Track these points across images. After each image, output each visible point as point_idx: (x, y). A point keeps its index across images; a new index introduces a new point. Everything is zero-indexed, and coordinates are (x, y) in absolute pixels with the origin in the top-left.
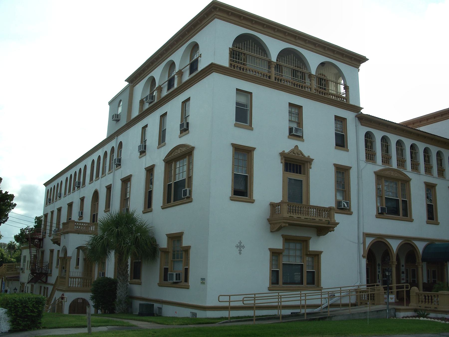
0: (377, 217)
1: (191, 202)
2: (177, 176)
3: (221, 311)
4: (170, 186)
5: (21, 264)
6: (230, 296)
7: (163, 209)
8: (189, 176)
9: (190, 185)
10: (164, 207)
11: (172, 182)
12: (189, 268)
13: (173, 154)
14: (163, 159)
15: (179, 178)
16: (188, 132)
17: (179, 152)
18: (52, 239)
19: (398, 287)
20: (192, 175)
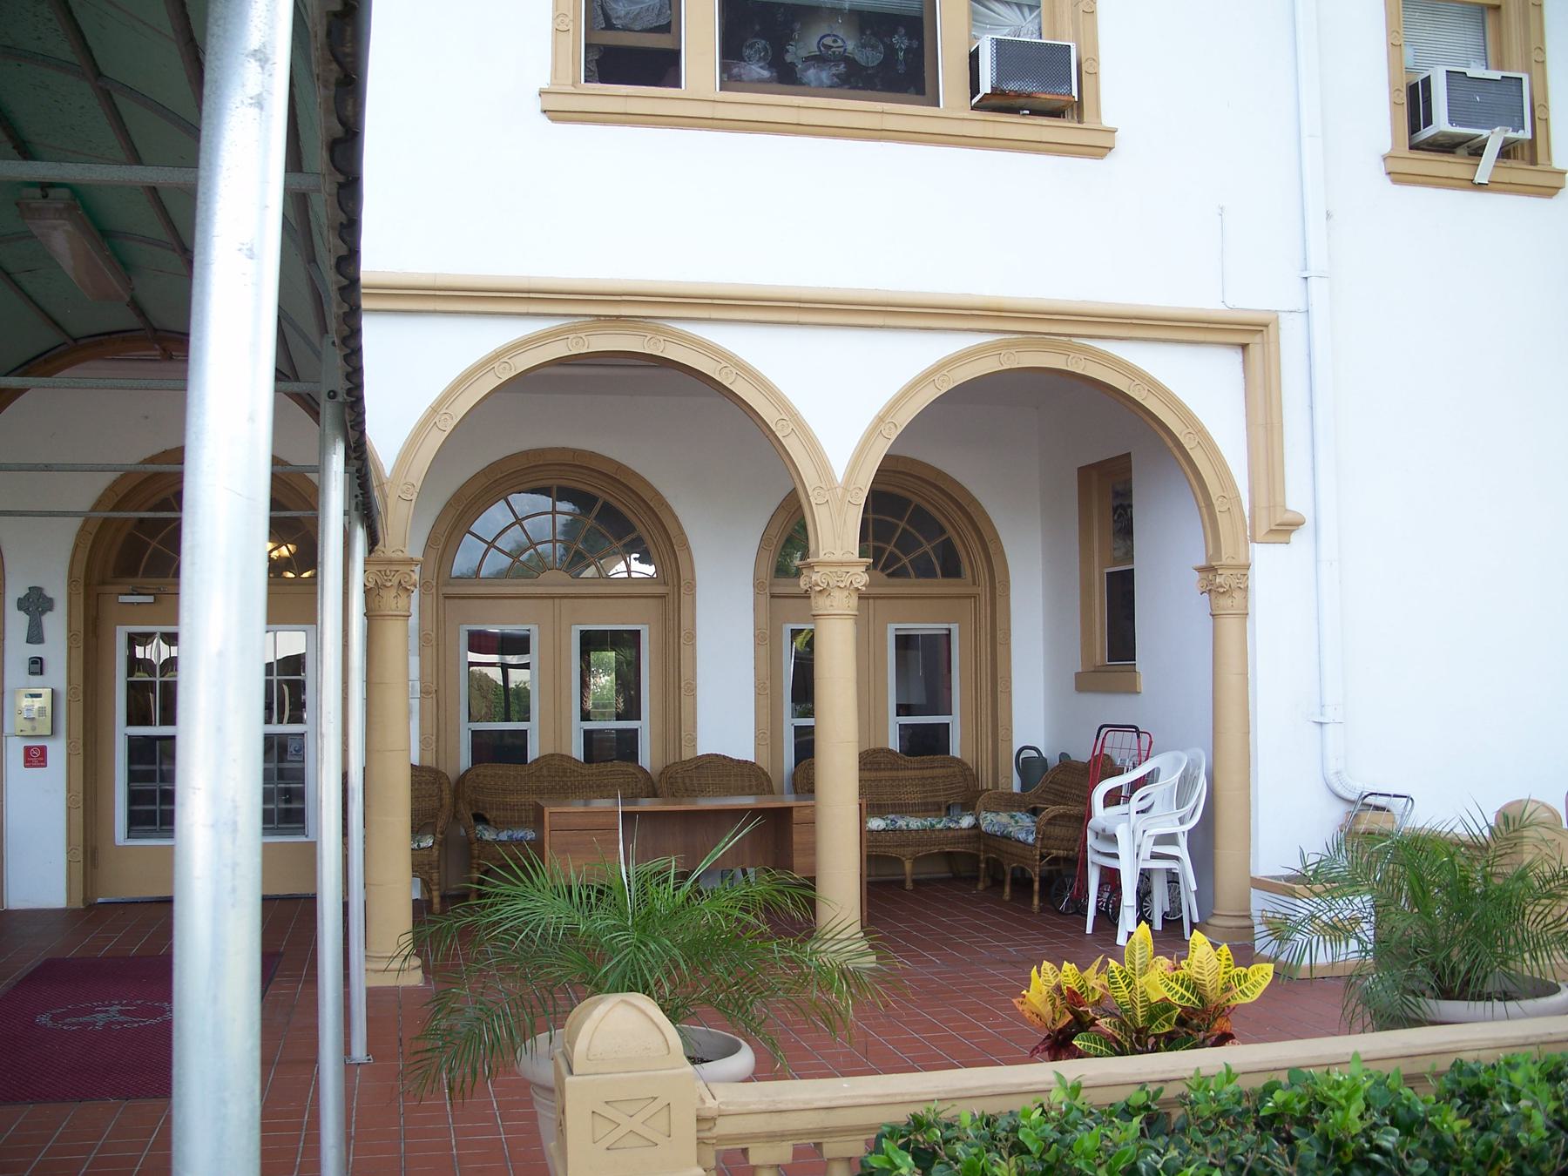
0: (1397, 177)
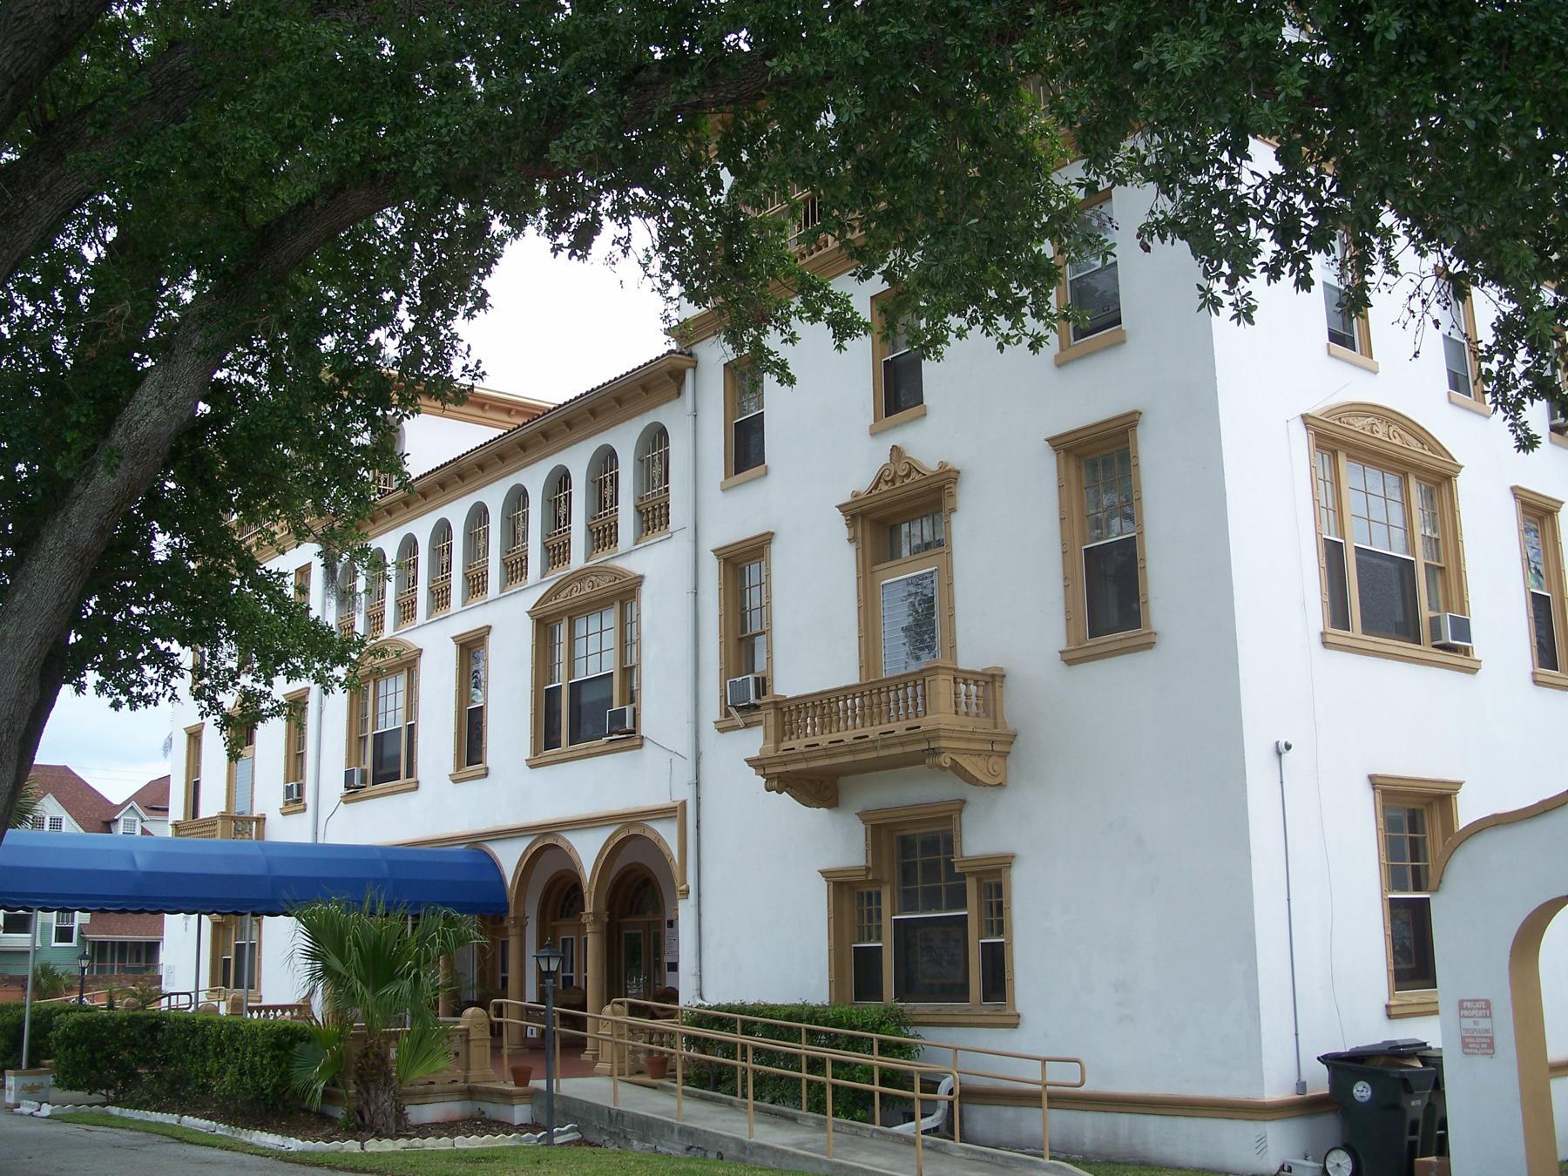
1: (1149, 645)
2: (381, 719)
3: (1251, 1123)
4: (552, 696)
5: (113, 943)
6: (1044, 1061)
7: (1070, 662)
8: (629, 665)
9: (631, 696)
10: (537, 762)
11: (562, 681)
12: (1011, 944)
13: (563, 594)
14: (529, 609)
15: (589, 669)
16: (763, 472)
17: (589, 590)
18: (758, 759)
19: (744, 1047)
20: (639, 659)
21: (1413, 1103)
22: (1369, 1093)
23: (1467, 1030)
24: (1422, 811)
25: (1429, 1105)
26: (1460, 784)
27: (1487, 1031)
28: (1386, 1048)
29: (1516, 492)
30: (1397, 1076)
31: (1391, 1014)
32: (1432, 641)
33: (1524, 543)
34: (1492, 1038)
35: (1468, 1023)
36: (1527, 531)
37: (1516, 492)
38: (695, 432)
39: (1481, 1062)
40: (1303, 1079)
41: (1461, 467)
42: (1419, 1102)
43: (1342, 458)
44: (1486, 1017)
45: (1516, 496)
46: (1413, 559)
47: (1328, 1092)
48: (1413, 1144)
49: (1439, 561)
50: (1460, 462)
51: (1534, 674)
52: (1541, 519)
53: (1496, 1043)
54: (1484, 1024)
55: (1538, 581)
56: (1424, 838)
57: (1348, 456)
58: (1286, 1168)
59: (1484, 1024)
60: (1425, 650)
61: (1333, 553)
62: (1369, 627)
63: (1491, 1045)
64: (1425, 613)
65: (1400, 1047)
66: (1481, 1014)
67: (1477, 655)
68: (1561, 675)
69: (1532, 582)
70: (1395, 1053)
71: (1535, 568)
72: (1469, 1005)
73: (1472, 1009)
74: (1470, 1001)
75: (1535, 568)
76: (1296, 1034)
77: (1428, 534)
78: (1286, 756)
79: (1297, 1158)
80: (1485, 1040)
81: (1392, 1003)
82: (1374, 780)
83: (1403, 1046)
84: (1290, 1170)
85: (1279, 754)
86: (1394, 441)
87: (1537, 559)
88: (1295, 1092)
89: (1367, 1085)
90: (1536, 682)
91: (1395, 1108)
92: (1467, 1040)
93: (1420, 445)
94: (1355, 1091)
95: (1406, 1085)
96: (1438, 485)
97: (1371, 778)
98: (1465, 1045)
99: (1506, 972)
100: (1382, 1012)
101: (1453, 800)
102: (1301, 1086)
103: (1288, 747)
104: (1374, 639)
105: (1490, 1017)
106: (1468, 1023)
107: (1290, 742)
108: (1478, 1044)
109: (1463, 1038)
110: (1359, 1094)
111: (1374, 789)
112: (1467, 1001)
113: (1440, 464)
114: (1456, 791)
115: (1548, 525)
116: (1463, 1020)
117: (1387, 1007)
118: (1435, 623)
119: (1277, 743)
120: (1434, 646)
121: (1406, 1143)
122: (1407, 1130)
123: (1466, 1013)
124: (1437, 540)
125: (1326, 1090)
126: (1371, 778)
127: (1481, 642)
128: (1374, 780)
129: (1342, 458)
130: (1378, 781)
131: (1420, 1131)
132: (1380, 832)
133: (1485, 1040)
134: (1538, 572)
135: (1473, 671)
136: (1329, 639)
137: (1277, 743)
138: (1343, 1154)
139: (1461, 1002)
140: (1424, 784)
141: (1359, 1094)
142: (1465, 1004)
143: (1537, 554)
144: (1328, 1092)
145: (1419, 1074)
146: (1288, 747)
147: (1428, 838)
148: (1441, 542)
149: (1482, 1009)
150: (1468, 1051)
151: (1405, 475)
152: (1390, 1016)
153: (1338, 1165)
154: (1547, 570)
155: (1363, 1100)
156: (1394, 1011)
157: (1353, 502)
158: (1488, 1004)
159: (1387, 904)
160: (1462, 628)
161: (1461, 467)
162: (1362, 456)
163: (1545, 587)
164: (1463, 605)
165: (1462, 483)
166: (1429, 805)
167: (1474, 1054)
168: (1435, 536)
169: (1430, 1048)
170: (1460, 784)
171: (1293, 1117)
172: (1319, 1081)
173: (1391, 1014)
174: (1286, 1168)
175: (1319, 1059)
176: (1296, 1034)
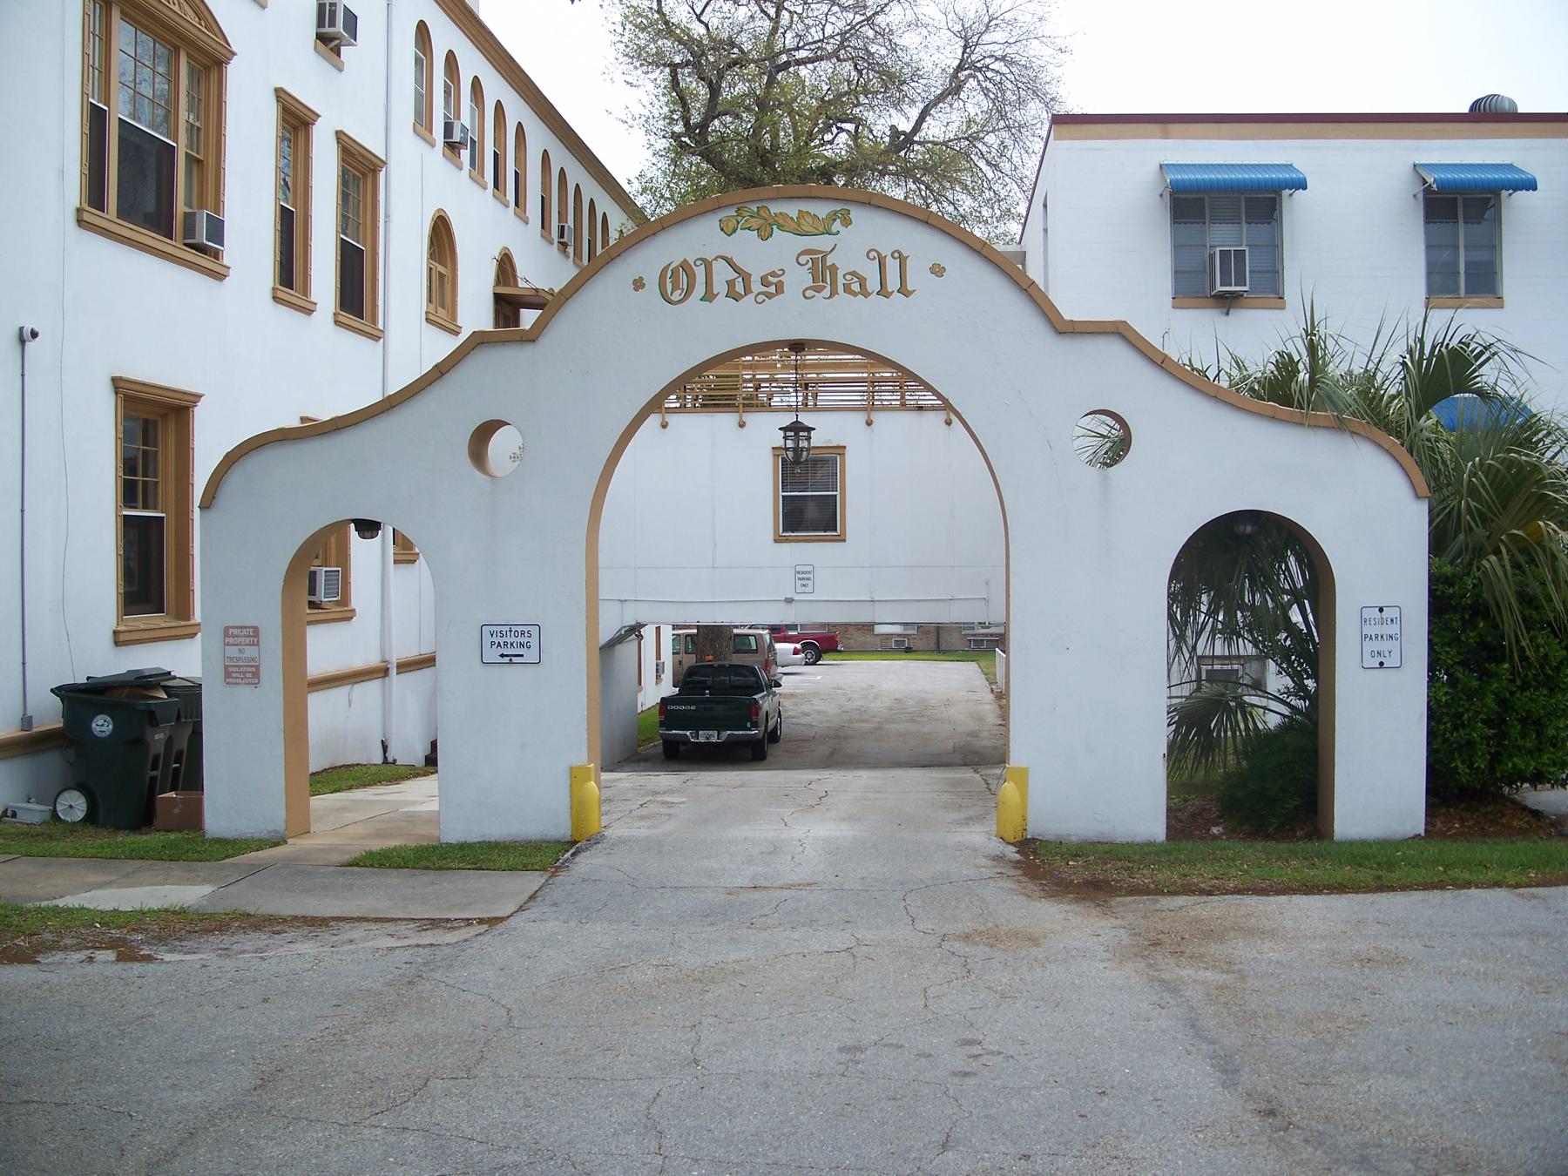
21: (157, 737)
22: (111, 727)
23: (231, 659)
24: (156, 422)
25: (170, 737)
26: (199, 396)
27: (253, 660)
28: (132, 678)
29: (280, 94)
30: (143, 708)
31: (119, 640)
32: (184, 239)
33: (280, 155)
34: (257, 667)
35: (233, 651)
36: (283, 139)
37: (280, 94)
38: (962, 242)
39: (244, 693)
40: (29, 713)
41: (234, 54)
42: (162, 735)
43: (116, 14)
44: (253, 645)
45: (278, 98)
46: (175, 145)
47: (61, 725)
48: (153, 779)
49: (198, 153)
50: (234, 48)
51: (274, 289)
52: (295, 129)
53: (221, 674)
54: (250, 652)
55: (284, 193)
56: (156, 452)
57: (122, 12)
58: (9, 813)
59: (250, 652)
60: (175, 246)
61: (96, 119)
62: (123, 213)
63: (256, 675)
64: (180, 207)
65: (146, 677)
66: (247, 641)
67: (226, 260)
68: (297, 294)
69: (281, 196)
70: (143, 683)
71: (284, 179)
72: (235, 631)
73: (237, 636)
74: (237, 627)
75: (284, 179)
76: (24, 664)
77: (191, 121)
78: (30, 346)
79: (18, 802)
80: (250, 669)
81: (119, 628)
82: (118, 384)
83: (150, 676)
84: (14, 815)
85: (22, 342)
86: (172, 6)
87: (286, 170)
88: (19, 728)
89: (109, 719)
90: (275, 298)
91: (139, 742)
92: (230, 669)
93: (197, 19)
94: (94, 725)
95: (152, 718)
96: (207, 69)
97: (114, 380)
98: (228, 674)
99: (279, 598)
100: (108, 638)
101: (191, 413)
102: (27, 721)
103: (34, 335)
104: (131, 226)
105: (258, 645)
106: (233, 651)
107: (36, 329)
108: (242, 673)
109: (226, 667)
110: (98, 728)
111: (116, 393)
112: (233, 627)
113: (214, 45)
114: (195, 403)
115: (301, 136)
116: (226, 647)
117: (115, 633)
118: (190, 219)
119: (21, 329)
120: (185, 245)
121: (148, 780)
122: (149, 766)
123: (231, 640)
124: (199, 129)
125: (58, 723)
126: (114, 380)
127: (231, 251)
128: (118, 384)
129: (116, 14)
130: (122, 385)
131: (160, 768)
132: (119, 441)
133: (250, 669)
134: (286, 183)
135: (220, 276)
136: (86, 217)
137: (21, 329)
138: (76, 794)
139: (227, 629)
140: (165, 393)
141: (98, 728)
142: (231, 631)
143: (287, 165)
144: (61, 725)
145: (165, 705)
146: (34, 335)
147: (160, 452)
148: (203, 131)
149: (249, 636)
150: (231, 680)
151: (177, 49)
152: (117, 643)
153: (71, 807)
154: (295, 183)
155: (103, 735)
156: (122, 638)
157: (121, 64)
158: (256, 630)
159: (120, 521)
160: (217, 230)
161: (234, 54)
162: (139, 18)
163: (290, 202)
164: (218, 204)
165: (233, 71)
166: (164, 416)
167: (237, 684)
168: (198, 124)
169: (175, 678)
170: (199, 396)
171: (12, 757)
172: (49, 713)
173: (119, 640)
174: (9, 813)
175: (52, 690)
176: (24, 664)
